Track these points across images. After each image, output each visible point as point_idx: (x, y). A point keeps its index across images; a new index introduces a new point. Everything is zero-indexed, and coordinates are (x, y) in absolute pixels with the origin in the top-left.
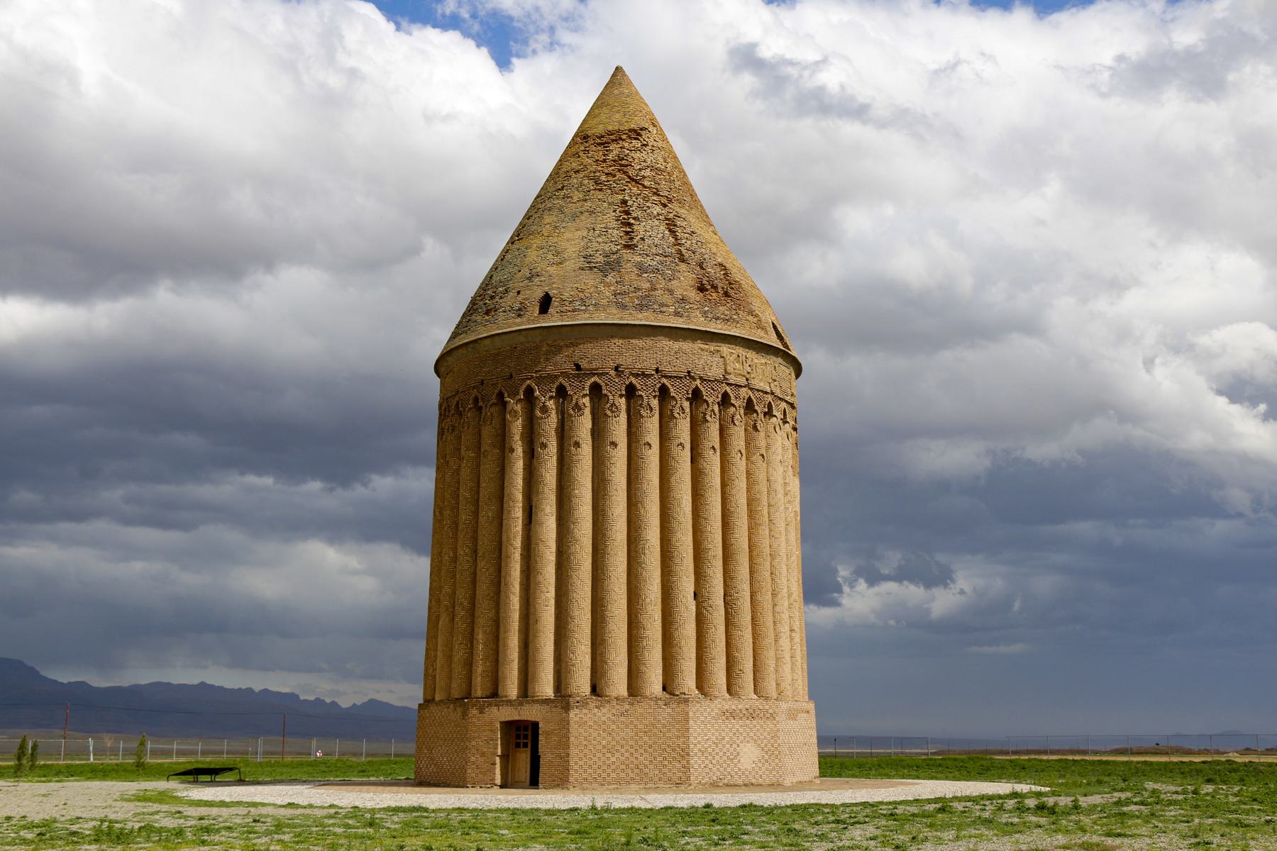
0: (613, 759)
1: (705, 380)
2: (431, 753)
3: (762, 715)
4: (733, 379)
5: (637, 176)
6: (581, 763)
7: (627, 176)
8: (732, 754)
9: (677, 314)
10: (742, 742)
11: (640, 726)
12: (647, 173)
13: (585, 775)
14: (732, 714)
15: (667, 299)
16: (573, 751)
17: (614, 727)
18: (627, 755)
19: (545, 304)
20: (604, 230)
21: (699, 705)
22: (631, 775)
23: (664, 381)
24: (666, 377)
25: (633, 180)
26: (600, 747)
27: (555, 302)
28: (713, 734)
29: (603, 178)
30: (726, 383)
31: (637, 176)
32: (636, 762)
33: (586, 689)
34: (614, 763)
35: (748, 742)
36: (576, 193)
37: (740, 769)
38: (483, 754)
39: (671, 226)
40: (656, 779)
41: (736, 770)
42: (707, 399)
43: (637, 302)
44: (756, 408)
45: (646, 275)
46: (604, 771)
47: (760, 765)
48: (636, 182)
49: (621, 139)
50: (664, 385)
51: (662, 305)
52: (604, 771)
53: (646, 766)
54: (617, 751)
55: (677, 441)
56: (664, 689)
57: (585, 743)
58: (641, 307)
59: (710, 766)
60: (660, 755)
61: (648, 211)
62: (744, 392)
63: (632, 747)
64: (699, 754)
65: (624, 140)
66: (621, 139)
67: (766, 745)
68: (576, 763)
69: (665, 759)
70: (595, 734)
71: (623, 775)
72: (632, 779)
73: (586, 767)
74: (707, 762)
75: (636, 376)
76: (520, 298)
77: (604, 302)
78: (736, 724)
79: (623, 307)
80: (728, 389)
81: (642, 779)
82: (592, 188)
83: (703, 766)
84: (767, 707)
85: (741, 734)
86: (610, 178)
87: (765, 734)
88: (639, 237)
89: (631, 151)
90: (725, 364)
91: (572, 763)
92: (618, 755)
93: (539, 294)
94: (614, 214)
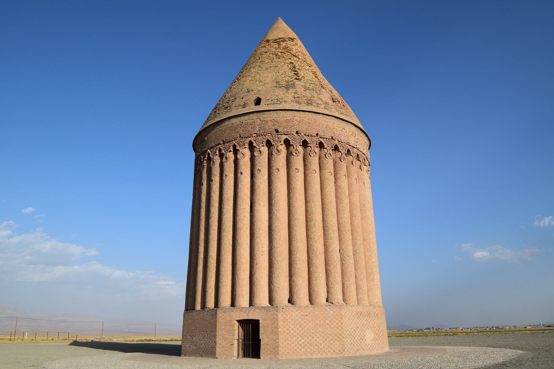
0: (303, 341)
2: (192, 339)
5: (295, 54)
6: (285, 343)
7: (291, 54)
9: (326, 108)
11: (317, 322)
12: (300, 54)
13: (288, 351)
14: (360, 314)
15: (319, 102)
16: (281, 336)
17: (303, 322)
18: (311, 338)
19: (258, 102)
20: (284, 72)
22: (314, 350)
23: (321, 140)
25: (294, 55)
26: (295, 334)
27: (263, 101)
28: (353, 325)
29: (280, 54)
30: (349, 145)
31: (295, 54)
32: (315, 342)
33: (247, 304)
34: (303, 343)
35: (369, 329)
36: (267, 60)
37: (366, 344)
38: (226, 339)
40: (327, 351)
43: (306, 101)
45: (308, 91)
46: (298, 348)
48: (295, 56)
49: (285, 41)
50: (321, 142)
51: (317, 104)
52: (298, 348)
53: (321, 344)
54: (305, 336)
55: (328, 171)
56: (327, 301)
57: (287, 331)
60: (328, 337)
61: (304, 67)
63: (313, 333)
65: (287, 41)
66: (285, 41)
67: (376, 331)
68: (282, 343)
69: (331, 340)
70: (292, 327)
71: (308, 350)
72: (314, 352)
73: (288, 346)
76: (244, 100)
77: (290, 100)
79: (298, 102)
81: (319, 352)
82: (274, 57)
86: (283, 54)
88: (302, 76)
89: (291, 45)
91: (280, 344)
92: (305, 338)
93: (254, 97)
94: (287, 67)
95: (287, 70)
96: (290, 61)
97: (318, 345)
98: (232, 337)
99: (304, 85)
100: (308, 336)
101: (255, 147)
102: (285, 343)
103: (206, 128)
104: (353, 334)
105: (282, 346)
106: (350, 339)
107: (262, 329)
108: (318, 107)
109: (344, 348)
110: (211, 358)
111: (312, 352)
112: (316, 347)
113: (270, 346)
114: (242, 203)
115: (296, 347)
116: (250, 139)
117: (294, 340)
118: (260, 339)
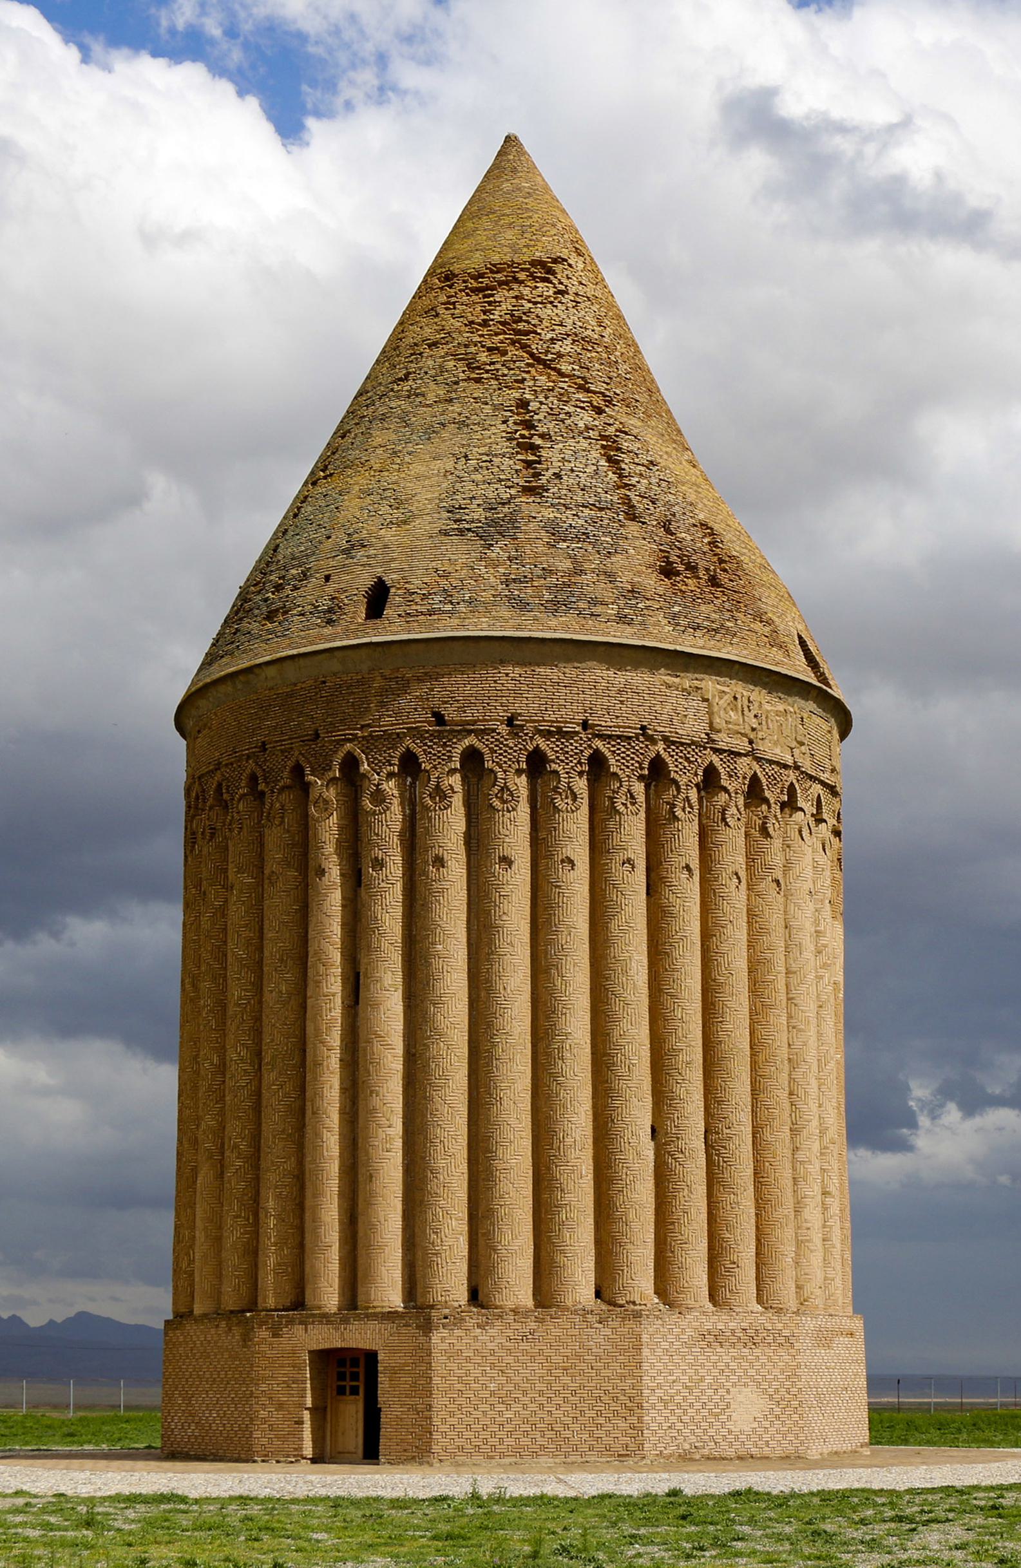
1: (674, 743)
2: (189, 1404)
3: (770, 1339)
4: (724, 740)
8: (717, 1405)
9: (622, 619)
10: (734, 1385)
12: (566, 347)
13: (459, 1442)
15: (603, 590)
18: (533, 1407)
21: (660, 1322)
23: (598, 744)
24: (601, 737)
25: (539, 361)
27: (395, 597)
28: (684, 1372)
29: (483, 357)
31: (546, 354)
37: (730, 1432)
39: (612, 451)
41: (724, 1432)
42: (677, 777)
43: (547, 596)
44: (767, 794)
45: (565, 545)
46: (493, 1435)
47: (766, 1424)
51: (594, 602)
55: (623, 856)
56: (598, 1294)
58: (555, 607)
59: (679, 1426)
61: (568, 422)
62: (745, 766)
64: (660, 1406)
68: (443, 1422)
69: (599, 1413)
71: (525, 1441)
74: (673, 1419)
75: (547, 735)
76: (330, 588)
78: (725, 1355)
80: (715, 759)
83: (665, 1426)
84: (780, 1326)
85: (734, 1371)
87: (776, 1372)
88: (551, 471)
89: (535, 303)
90: (710, 714)
91: (436, 1421)
92: (517, 1407)
93: (365, 580)
95: (504, 447)
96: (517, 395)
97: (558, 1427)
98: (297, 1399)
99: (551, 515)
100: (526, 1400)
101: (364, 776)
102: (452, 1419)
103: (206, 687)
104: (678, 1399)
105: (443, 1428)
106: (666, 1413)
107: (384, 1379)
108: (592, 615)
109: (641, 1438)
110: (631, 1496)
111: (536, 1448)
112: (550, 1434)
113: (406, 1427)
114: (324, 977)
115: (485, 1433)
116: (467, 742)
117: (579, 1412)
118: (380, 1408)
